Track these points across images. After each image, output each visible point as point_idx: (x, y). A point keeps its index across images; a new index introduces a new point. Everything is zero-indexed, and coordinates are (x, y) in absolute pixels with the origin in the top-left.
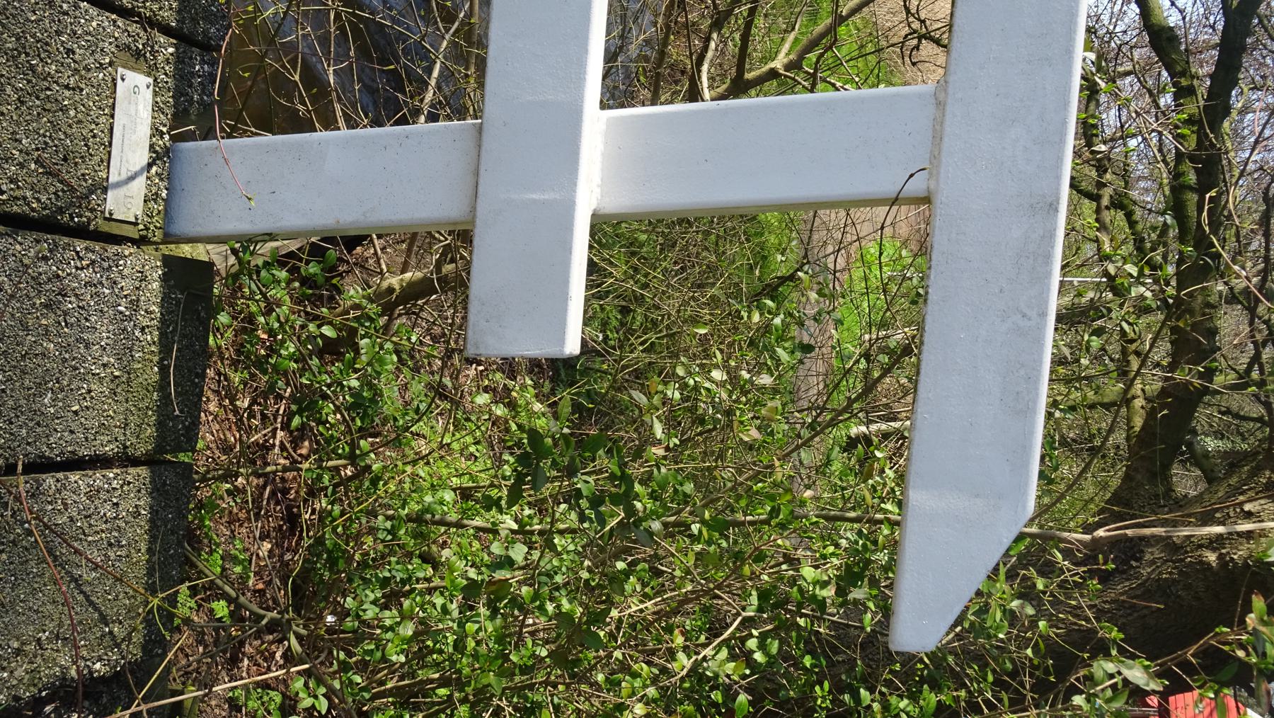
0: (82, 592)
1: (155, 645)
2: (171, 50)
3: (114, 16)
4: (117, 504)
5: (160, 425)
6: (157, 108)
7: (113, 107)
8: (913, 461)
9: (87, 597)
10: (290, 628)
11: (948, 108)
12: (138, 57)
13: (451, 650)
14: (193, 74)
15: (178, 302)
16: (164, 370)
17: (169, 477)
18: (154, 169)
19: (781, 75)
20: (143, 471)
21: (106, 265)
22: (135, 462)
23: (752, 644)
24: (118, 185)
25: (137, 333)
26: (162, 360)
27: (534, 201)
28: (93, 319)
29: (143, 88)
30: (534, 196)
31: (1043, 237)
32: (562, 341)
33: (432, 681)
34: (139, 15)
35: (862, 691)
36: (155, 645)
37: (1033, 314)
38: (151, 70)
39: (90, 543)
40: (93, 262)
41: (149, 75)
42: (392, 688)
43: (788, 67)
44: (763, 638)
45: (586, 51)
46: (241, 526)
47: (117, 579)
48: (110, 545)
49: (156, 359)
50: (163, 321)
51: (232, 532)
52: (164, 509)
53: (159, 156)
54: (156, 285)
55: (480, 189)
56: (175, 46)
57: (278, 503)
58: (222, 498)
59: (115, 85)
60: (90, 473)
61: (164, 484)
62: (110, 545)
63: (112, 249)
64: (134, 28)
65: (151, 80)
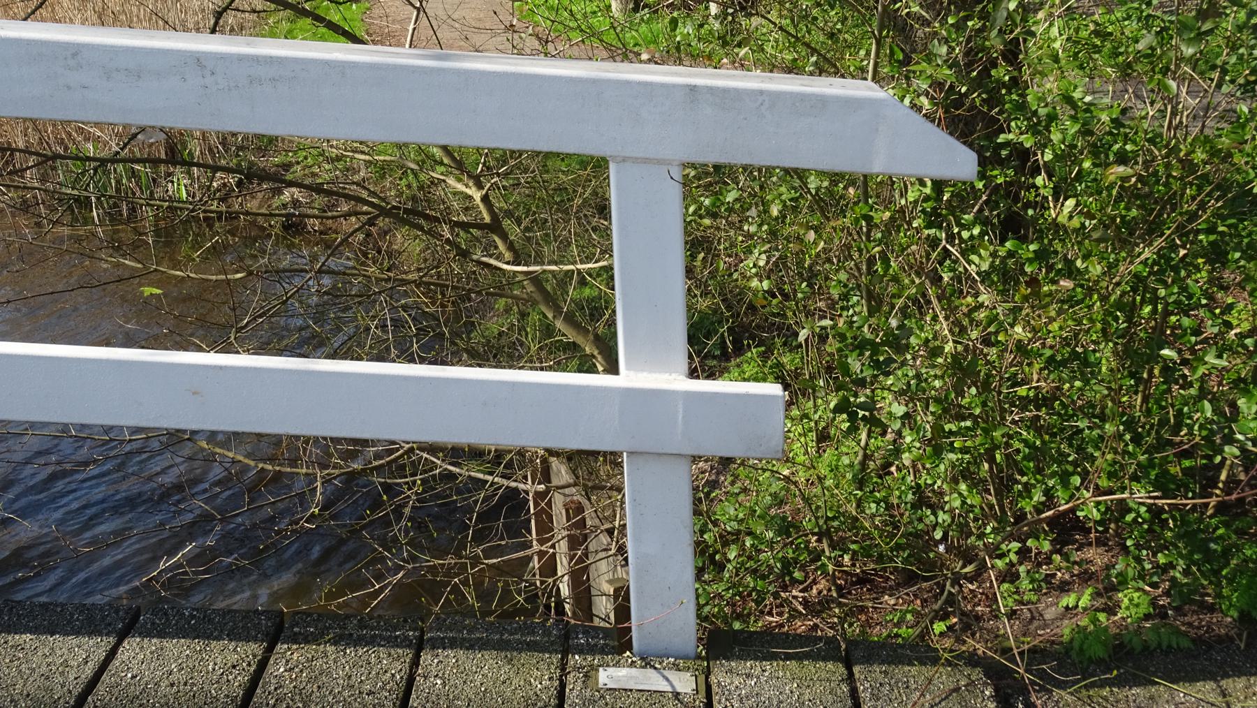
0: (940, 703)
1: (972, 660)
2: (577, 657)
3: (567, 690)
4: (881, 684)
5: (825, 659)
6: (617, 665)
7: (626, 690)
8: (853, 170)
9: (943, 700)
10: (958, 572)
11: (627, 155)
12: (589, 675)
13: (967, 456)
14: (588, 644)
15: (740, 650)
16: (788, 657)
17: (858, 654)
18: (657, 666)
19: (487, 193)
20: (856, 669)
21: (726, 693)
22: (851, 674)
23: (965, 235)
24: (672, 686)
25: (767, 674)
26: (781, 659)
27: (683, 417)
28: (763, 699)
29: (607, 673)
30: (680, 417)
31: (712, 94)
32: (774, 397)
33: (991, 468)
34: (561, 676)
35: (999, 141)
36: (972, 660)
37: (761, 99)
38: (595, 669)
39: (908, 699)
40: (726, 699)
41: (597, 671)
42: (997, 499)
43: (480, 186)
44: (963, 227)
45: (588, 386)
46: (872, 618)
47: (930, 683)
48: (907, 687)
49: (781, 663)
50: (756, 659)
51: (877, 624)
52: (880, 656)
53: (647, 662)
54: (733, 664)
55: (675, 452)
56: (573, 655)
57: (850, 593)
58: (854, 631)
59: (610, 689)
60: (861, 700)
61: (863, 656)
62: (907, 687)
63: (715, 688)
64: (570, 678)
65: (601, 669)
